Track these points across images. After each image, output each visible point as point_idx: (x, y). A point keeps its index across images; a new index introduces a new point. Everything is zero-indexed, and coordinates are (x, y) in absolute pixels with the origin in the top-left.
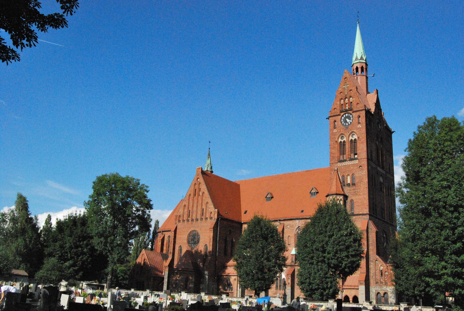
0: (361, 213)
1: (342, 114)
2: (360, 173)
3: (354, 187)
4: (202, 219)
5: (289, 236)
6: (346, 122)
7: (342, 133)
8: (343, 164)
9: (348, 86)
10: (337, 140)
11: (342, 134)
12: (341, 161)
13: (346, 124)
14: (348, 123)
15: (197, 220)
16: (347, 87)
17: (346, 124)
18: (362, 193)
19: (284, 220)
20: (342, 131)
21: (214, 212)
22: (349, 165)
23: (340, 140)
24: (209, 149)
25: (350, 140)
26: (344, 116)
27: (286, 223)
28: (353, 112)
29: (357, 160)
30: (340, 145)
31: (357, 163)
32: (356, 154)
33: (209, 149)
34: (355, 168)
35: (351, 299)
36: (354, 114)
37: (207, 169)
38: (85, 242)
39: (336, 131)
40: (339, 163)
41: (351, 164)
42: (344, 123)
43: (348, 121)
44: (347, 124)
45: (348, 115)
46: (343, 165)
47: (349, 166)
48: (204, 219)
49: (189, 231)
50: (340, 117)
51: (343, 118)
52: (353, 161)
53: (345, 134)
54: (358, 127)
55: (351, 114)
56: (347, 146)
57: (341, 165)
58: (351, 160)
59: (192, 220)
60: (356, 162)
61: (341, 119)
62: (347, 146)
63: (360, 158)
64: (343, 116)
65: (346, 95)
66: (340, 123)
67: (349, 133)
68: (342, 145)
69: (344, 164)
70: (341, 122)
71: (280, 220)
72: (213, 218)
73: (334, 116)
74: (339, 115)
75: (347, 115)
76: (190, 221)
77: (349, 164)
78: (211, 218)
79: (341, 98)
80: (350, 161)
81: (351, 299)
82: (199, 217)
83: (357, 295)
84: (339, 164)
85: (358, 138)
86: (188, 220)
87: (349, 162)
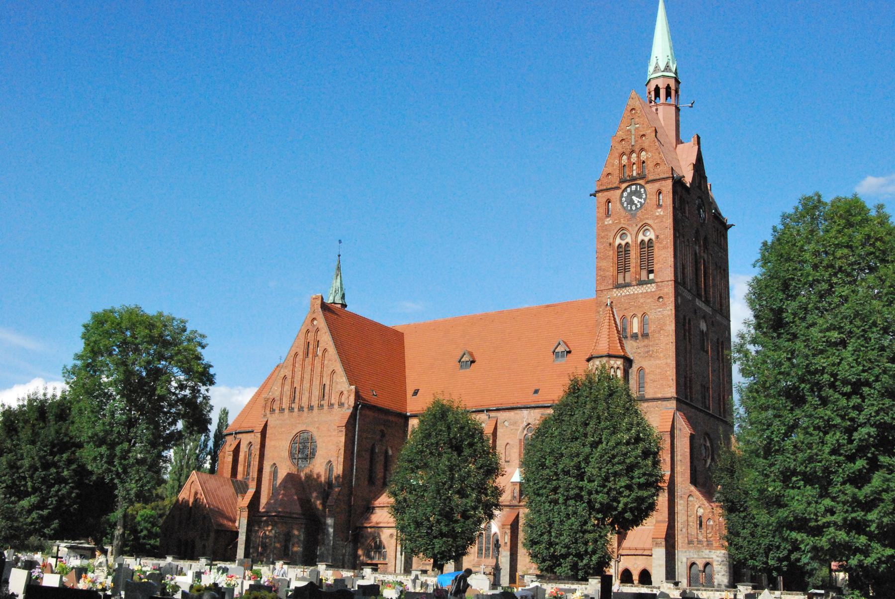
0: (659, 396)
1: (624, 186)
3: (646, 342)
4: (322, 406)
5: (508, 443)
6: (631, 202)
9: (638, 125)
10: (611, 241)
11: (622, 229)
12: (618, 286)
13: (631, 207)
14: (636, 205)
15: (311, 408)
17: (631, 207)
18: (662, 355)
19: (498, 410)
20: (622, 221)
23: (618, 241)
24: (339, 256)
25: (639, 241)
26: (629, 190)
27: (501, 415)
28: (647, 182)
29: (653, 285)
30: (618, 252)
31: (653, 290)
35: (636, 577)
36: (648, 186)
37: (334, 300)
38: (65, 456)
39: (610, 222)
40: (615, 290)
42: (627, 204)
43: (636, 202)
44: (634, 208)
45: (636, 188)
46: (623, 294)
47: (635, 297)
48: (326, 407)
49: (294, 432)
50: (619, 192)
51: (625, 194)
53: (630, 229)
54: (657, 214)
55: (642, 186)
56: (634, 254)
57: (619, 294)
58: (641, 283)
59: (301, 409)
60: (652, 288)
61: (622, 196)
62: (634, 254)
63: (659, 280)
65: (632, 146)
66: (618, 204)
67: (638, 227)
68: (623, 251)
70: (622, 204)
71: (488, 411)
72: (346, 406)
73: (607, 190)
74: (617, 188)
75: (634, 187)
76: (296, 410)
78: (341, 405)
79: (621, 151)
81: (636, 577)
82: (315, 403)
83: (648, 569)
84: (616, 293)
85: (657, 237)
86: (321, 407)
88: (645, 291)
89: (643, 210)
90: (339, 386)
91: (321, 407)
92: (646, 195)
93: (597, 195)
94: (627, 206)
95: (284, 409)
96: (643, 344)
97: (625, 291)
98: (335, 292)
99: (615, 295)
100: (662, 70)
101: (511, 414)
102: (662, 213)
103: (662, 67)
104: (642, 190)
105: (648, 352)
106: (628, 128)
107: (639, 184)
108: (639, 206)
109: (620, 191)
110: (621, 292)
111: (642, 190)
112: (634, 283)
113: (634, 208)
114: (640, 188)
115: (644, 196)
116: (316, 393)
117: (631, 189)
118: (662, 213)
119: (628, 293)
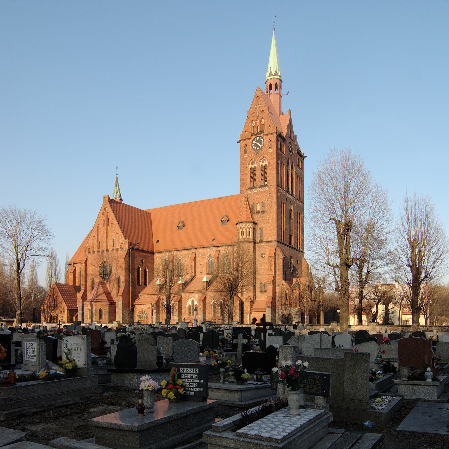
0: (269, 240)
1: (253, 137)
2: (269, 200)
4: (113, 249)
7: (253, 158)
9: (260, 105)
13: (257, 149)
16: (260, 107)
17: (257, 149)
21: (125, 242)
24: (117, 175)
25: (260, 165)
26: (256, 139)
28: (264, 136)
29: (267, 187)
31: (267, 190)
33: (117, 175)
40: (249, 190)
41: (261, 191)
42: (255, 147)
44: (258, 149)
45: (259, 139)
47: (258, 193)
50: (251, 140)
52: (263, 188)
54: (269, 152)
60: (266, 189)
63: (269, 185)
64: (254, 140)
67: (260, 158)
68: (253, 171)
70: (252, 147)
73: (245, 139)
74: (250, 138)
77: (259, 191)
84: (249, 192)
85: (269, 163)
87: (259, 189)
88: (263, 190)
89: (262, 150)
90: (120, 240)
91: (112, 250)
92: (264, 142)
93: (240, 142)
94: (255, 148)
95: (95, 252)
96: (262, 216)
97: (258, 190)
98: (116, 193)
99: (249, 192)
100: (273, 74)
102: (271, 151)
103: (273, 73)
105: (264, 219)
106: (255, 107)
110: (252, 191)
112: (258, 186)
113: (258, 149)
115: (253, 144)
116: (110, 243)
119: (255, 191)
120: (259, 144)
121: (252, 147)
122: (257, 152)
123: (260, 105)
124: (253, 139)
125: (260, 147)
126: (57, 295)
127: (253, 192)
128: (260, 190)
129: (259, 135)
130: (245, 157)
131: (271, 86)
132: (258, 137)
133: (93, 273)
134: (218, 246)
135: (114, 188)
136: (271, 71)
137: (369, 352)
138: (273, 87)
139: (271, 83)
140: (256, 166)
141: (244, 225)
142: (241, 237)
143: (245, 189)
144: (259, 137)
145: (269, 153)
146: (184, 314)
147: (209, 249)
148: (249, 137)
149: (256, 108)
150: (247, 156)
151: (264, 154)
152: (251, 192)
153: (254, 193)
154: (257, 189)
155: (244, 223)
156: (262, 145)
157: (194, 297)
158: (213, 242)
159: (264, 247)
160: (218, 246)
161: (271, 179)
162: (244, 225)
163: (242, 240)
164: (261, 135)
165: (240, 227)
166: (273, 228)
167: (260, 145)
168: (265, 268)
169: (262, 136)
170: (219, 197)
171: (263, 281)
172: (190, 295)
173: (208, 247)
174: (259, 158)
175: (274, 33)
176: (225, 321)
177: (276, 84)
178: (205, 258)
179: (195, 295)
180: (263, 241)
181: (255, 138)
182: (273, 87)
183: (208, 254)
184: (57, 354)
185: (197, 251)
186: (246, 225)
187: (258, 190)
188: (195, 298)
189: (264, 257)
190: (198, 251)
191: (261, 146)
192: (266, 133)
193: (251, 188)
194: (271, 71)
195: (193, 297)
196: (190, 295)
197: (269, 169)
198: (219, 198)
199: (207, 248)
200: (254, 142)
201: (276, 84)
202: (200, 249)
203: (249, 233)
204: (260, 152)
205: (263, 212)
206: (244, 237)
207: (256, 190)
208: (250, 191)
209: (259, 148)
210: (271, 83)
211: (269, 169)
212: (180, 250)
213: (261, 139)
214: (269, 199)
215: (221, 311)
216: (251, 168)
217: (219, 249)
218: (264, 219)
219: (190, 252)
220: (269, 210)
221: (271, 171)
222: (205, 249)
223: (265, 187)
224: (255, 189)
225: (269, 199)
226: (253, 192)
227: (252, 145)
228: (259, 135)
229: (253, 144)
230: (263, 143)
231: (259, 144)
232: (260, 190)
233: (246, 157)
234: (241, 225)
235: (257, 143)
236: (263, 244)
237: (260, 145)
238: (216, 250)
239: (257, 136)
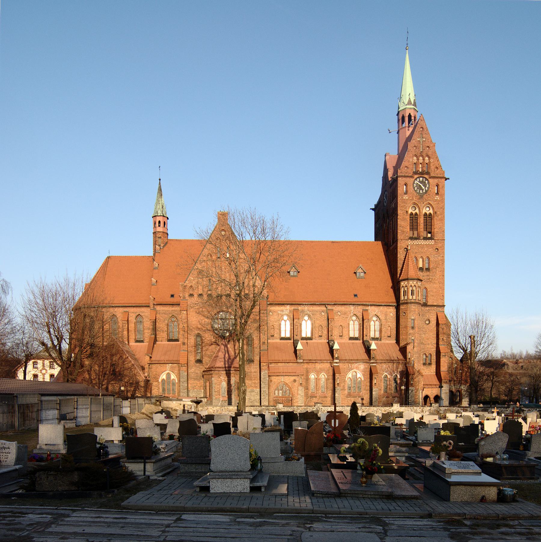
0: (435, 304)
1: (416, 176)
2: (436, 257)
3: (428, 273)
8: (415, 242)
9: (424, 139)
11: (415, 203)
13: (419, 191)
17: (419, 191)
22: (423, 245)
23: (410, 211)
24: (160, 180)
25: (423, 213)
26: (418, 179)
28: (430, 178)
29: (433, 241)
31: (433, 244)
32: (430, 233)
33: (160, 180)
34: (430, 250)
39: (407, 198)
40: (410, 240)
41: (425, 243)
42: (417, 189)
44: (421, 192)
45: (423, 180)
47: (422, 246)
52: (428, 241)
54: (436, 199)
55: (426, 179)
56: (421, 220)
57: (412, 243)
58: (426, 238)
60: (432, 242)
62: (421, 220)
64: (416, 179)
69: (416, 242)
70: (414, 188)
74: (412, 177)
77: (422, 243)
80: (425, 239)
84: (410, 242)
87: (422, 240)
88: (428, 244)
89: (427, 194)
92: (429, 186)
97: (421, 242)
98: (162, 208)
101: (343, 308)
102: (438, 199)
104: (427, 182)
105: (429, 279)
106: (418, 139)
107: (425, 178)
108: (424, 191)
109: (414, 179)
110: (414, 242)
111: (427, 182)
114: (425, 181)
117: (419, 179)
118: (438, 199)
119: (417, 243)
120: (422, 186)
121: (414, 188)
122: (420, 196)
123: (424, 139)
124: (415, 178)
125: (424, 190)
126: (121, 356)
127: (415, 243)
128: (424, 242)
129: (423, 176)
130: (404, 198)
131: (403, 118)
132: (421, 177)
133: (199, 326)
134: (365, 305)
135: (156, 198)
136: (409, 98)
137: (215, 420)
138: (407, 119)
139: (410, 114)
140: (418, 213)
141: (415, 283)
142: (410, 297)
143: (404, 238)
144: (423, 177)
145: (436, 200)
146: (446, 393)
147: (352, 307)
148: (410, 175)
149: (419, 141)
150: (407, 198)
151: (430, 200)
152: (412, 243)
153: (416, 245)
154: (420, 241)
155: (415, 280)
156: (427, 189)
157: (357, 368)
158: (355, 299)
159: (429, 312)
160: (365, 305)
161: (438, 231)
162: (415, 283)
163: (413, 301)
164: (426, 176)
165: (410, 285)
166: (441, 290)
167: (423, 188)
168: (430, 337)
169: (428, 178)
170: (333, 241)
171: (428, 352)
172: (351, 366)
173: (352, 305)
174: (423, 203)
175: (408, 53)
176: (410, 399)
177: (410, 116)
178: (347, 318)
179: (359, 366)
180: (428, 304)
181: (418, 178)
182: (407, 119)
183: (352, 314)
184: (304, 458)
185: (334, 308)
186: (417, 283)
187: (421, 242)
188: (358, 369)
189: (427, 324)
190: (336, 308)
191: (425, 190)
192: (432, 175)
193: (411, 238)
194: (409, 98)
195: (357, 368)
196: (351, 366)
197: (436, 219)
198: (333, 242)
199: (351, 306)
200: (416, 182)
201: (410, 116)
202: (340, 306)
203: (413, 293)
204: (425, 196)
205: (428, 269)
206: (414, 297)
207: (419, 242)
208: (411, 242)
209: (423, 191)
210: (410, 114)
211: (436, 219)
212: (310, 305)
213: (425, 181)
214: (436, 256)
215: (396, 386)
216: (412, 214)
217: (367, 308)
218: (429, 279)
219: (323, 308)
220: (436, 269)
221: (439, 222)
222: (348, 306)
223: (430, 241)
224: (417, 241)
225: (436, 256)
226: (415, 243)
227: (413, 185)
228: (423, 176)
229: (415, 185)
230: (428, 186)
231: (422, 186)
232: (424, 242)
233: (406, 199)
234: (411, 283)
235: (420, 184)
236: (428, 308)
237: (423, 188)
238: (363, 310)
239: (420, 176)
